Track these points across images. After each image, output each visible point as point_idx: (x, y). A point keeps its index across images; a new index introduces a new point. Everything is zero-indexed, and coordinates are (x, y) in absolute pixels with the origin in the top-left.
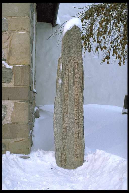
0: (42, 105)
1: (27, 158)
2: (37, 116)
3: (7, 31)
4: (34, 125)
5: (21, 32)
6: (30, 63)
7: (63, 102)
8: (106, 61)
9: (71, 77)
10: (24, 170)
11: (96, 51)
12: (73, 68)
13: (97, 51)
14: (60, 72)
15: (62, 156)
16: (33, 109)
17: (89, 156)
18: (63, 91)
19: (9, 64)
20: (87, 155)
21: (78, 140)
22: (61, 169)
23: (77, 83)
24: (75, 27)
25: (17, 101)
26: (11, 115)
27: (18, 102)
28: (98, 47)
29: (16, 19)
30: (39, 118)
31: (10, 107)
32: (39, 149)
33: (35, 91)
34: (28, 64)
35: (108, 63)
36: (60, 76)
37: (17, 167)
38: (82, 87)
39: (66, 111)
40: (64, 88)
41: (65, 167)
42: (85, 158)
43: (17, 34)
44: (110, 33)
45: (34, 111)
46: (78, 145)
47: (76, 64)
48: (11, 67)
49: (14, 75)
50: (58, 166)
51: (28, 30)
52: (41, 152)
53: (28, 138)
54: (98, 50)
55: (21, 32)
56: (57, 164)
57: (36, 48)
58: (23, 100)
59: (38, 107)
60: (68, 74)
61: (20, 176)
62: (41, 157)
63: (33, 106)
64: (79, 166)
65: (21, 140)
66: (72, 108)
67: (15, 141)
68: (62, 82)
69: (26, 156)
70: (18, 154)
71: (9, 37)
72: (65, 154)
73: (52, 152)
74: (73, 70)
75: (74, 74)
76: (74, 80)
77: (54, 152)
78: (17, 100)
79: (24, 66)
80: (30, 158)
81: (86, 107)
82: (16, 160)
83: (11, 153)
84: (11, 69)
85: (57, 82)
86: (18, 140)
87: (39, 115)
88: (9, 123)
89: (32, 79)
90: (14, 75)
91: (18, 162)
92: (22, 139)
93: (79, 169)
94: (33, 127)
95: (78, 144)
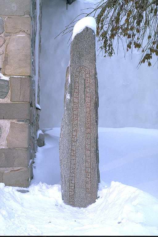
0: (50, 129)
1: (26, 192)
2: (41, 143)
3: (3, 33)
4: (35, 155)
5: (20, 35)
6: (30, 73)
7: (72, 122)
8: (145, 61)
9: (81, 92)
10: (22, 205)
11: (127, 49)
12: (84, 80)
13: (129, 49)
14: (68, 84)
15: (70, 190)
16: (35, 133)
17: (103, 192)
18: (72, 109)
19: (4, 75)
20: (102, 190)
21: (90, 170)
22: (68, 207)
23: (89, 98)
24: (86, 29)
25: (14, 121)
26: (6, 138)
27: (16, 122)
28: (131, 43)
29: (13, 18)
30: (44, 146)
31: (6, 128)
32: (41, 182)
33: (38, 106)
34: (28, 75)
35: (150, 64)
36: (69, 90)
37: (13, 201)
38: (95, 104)
39: (74, 134)
40: (73, 105)
41: (73, 205)
42: (99, 193)
43: (14, 37)
44: (147, 23)
45: (36, 135)
46: (89, 177)
47: (88, 76)
48: (7, 78)
49: (10, 89)
50: (64, 203)
51: (29, 32)
52: (44, 186)
53: (27, 167)
54: (130, 48)
55: (20, 35)
56: (63, 201)
57: (40, 38)
58: (22, 119)
59: (43, 131)
60: (77, 87)
61: (16, 210)
62: (43, 192)
63: (36, 129)
64: (90, 203)
65: (19, 170)
66: (83, 129)
67: (11, 171)
68: (70, 98)
69: (25, 189)
70: (15, 187)
71: (5, 40)
72: (73, 188)
73: (58, 186)
74: (85, 82)
75: (85, 88)
76: (85, 95)
77: (60, 186)
78: (14, 119)
79: (24, 77)
80: (29, 192)
81: (100, 130)
82: (12, 193)
83: (6, 185)
84: (7, 81)
85: (65, 97)
86: (16, 169)
87: (44, 143)
88: (3, 148)
89: (34, 90)
90: (10, 89)
91: (14, 196)
92: (19, 168)
93: (91, 207)
94: (35, 157)
95: (90, 175)
